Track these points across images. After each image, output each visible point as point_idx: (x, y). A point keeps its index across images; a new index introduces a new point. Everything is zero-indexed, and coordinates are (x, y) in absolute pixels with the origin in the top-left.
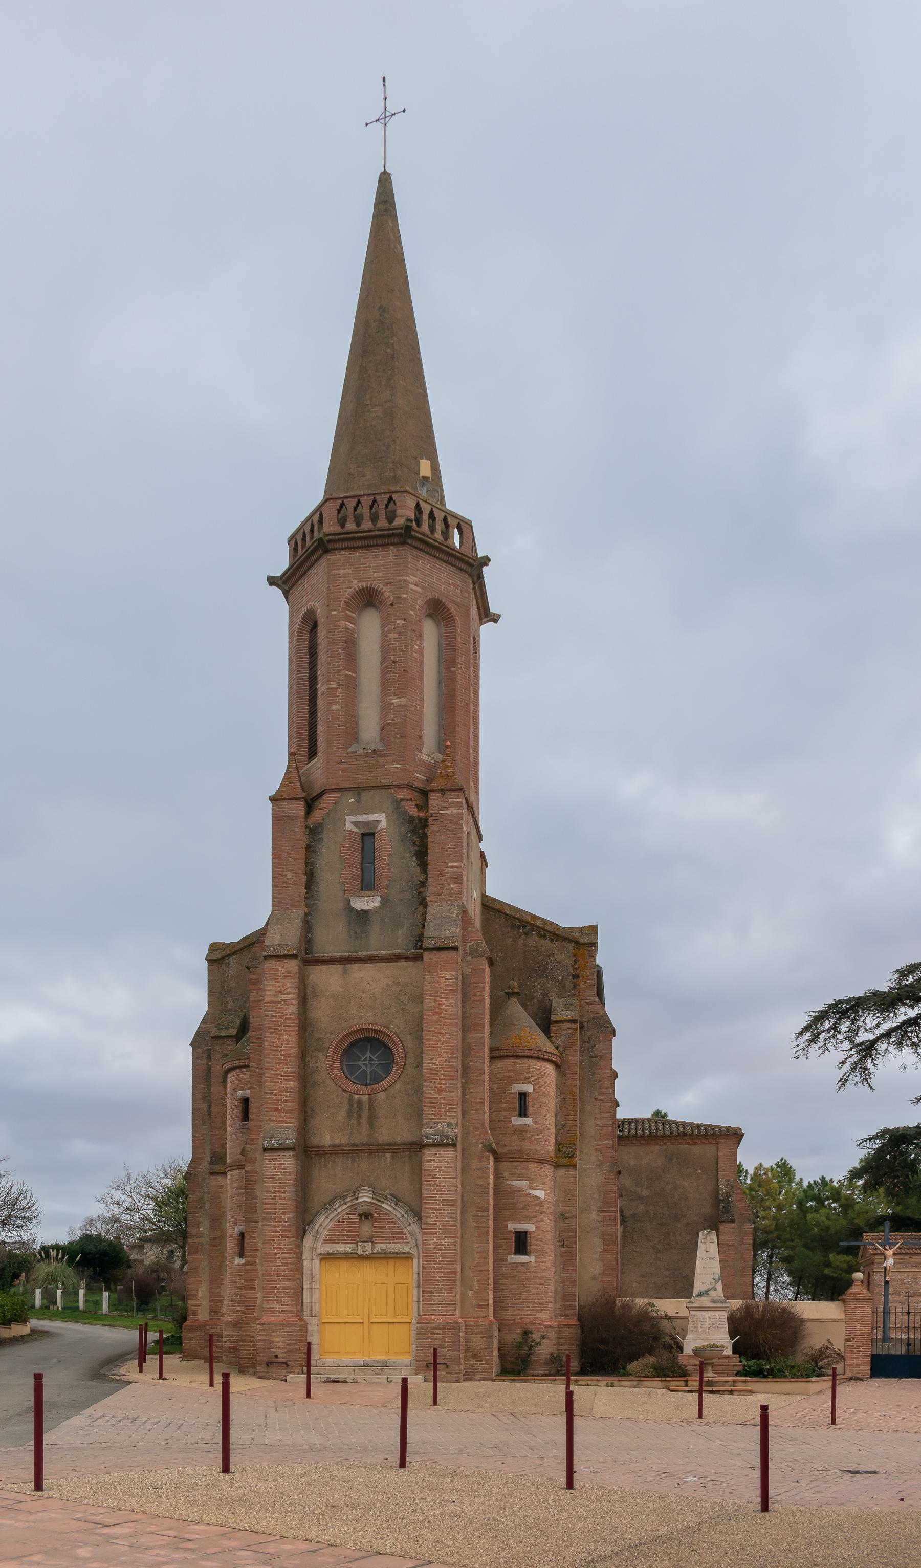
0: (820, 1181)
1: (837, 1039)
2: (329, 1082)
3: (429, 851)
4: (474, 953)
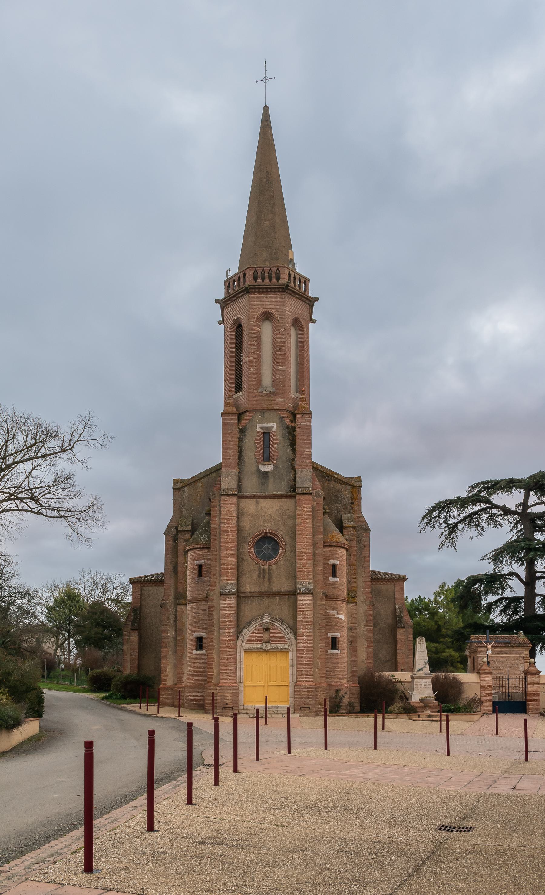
0: (418, 599)
1: (440, 522)
2: (249, 559)
3: (296, 443)
4: (318, 495)
